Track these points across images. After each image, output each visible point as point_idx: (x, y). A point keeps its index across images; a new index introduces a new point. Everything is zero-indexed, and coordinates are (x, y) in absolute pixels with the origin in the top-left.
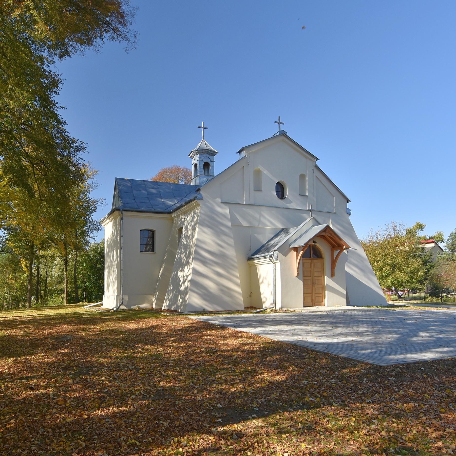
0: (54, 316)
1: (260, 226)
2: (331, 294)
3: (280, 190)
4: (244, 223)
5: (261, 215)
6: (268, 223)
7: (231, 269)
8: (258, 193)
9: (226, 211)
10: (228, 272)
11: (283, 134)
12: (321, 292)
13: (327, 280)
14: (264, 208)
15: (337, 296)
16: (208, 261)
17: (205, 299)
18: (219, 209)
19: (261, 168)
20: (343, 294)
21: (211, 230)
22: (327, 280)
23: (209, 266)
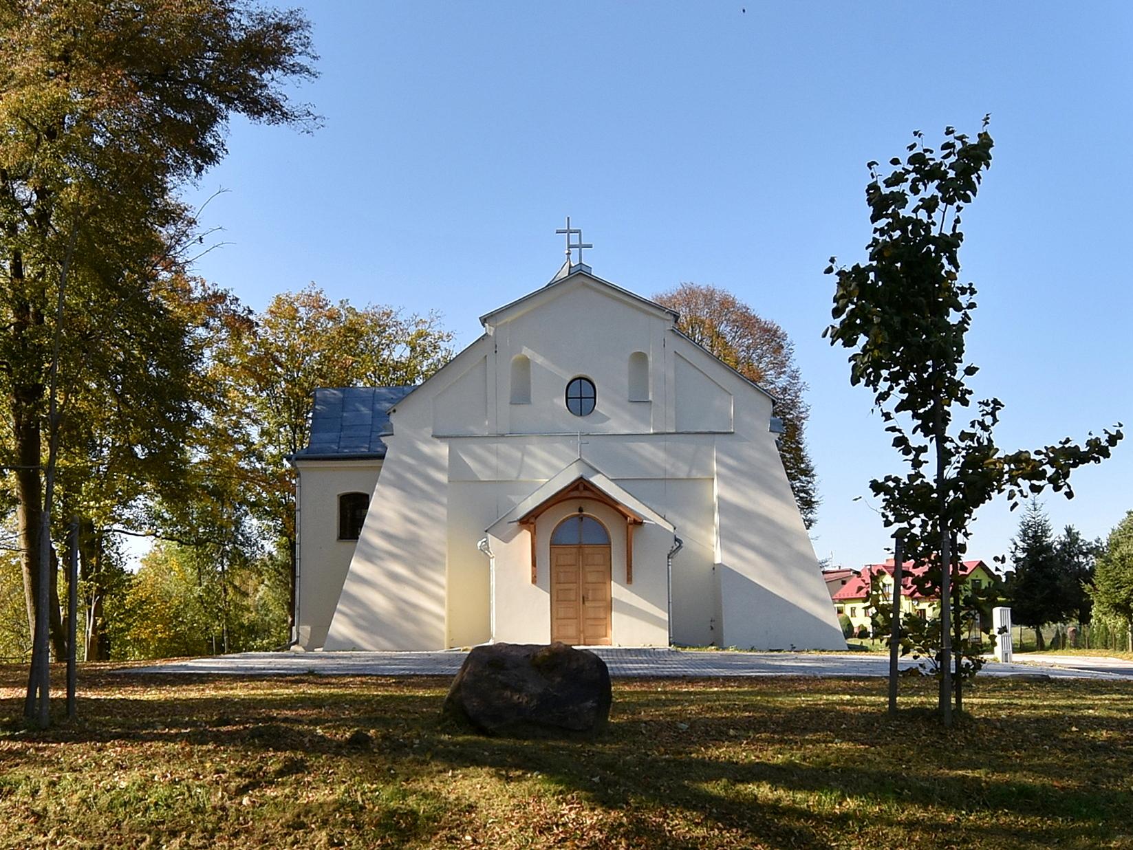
0: (402, 680)
1: (522, 478)
2: (626, 618)
3: (581, 395)
4: (484, 475)
5: (525, 452)
6: (540, 467)
7: (425, 566)
8: (521, 410)
9: (443, 450)
10: (416, 572)
11: (580, 273)
12: (602, 616)
13: (617, 590)
14: (534, 439)
15: (634, 620)
16: (378, 553)
17: (357, 626)
18: (426, 449)
19: (527, 352)
20: (835, 630)
21: (398, 492)
22: (617, 590)
23: (379, 562)
